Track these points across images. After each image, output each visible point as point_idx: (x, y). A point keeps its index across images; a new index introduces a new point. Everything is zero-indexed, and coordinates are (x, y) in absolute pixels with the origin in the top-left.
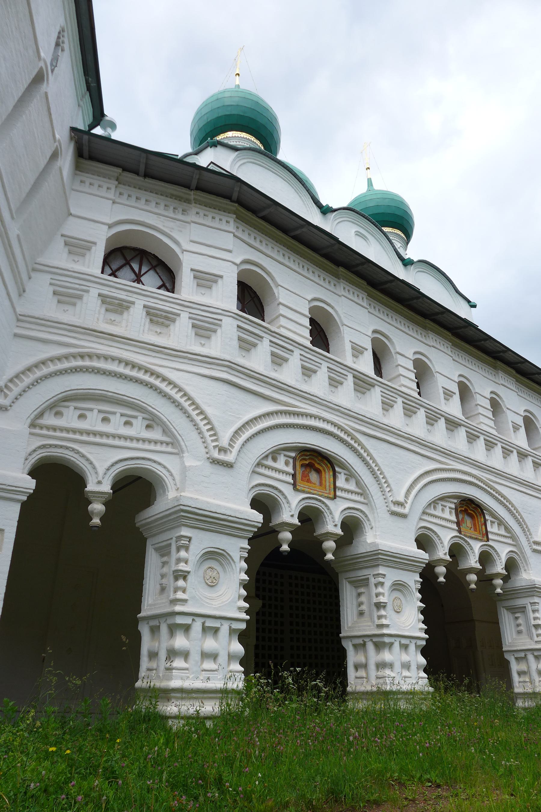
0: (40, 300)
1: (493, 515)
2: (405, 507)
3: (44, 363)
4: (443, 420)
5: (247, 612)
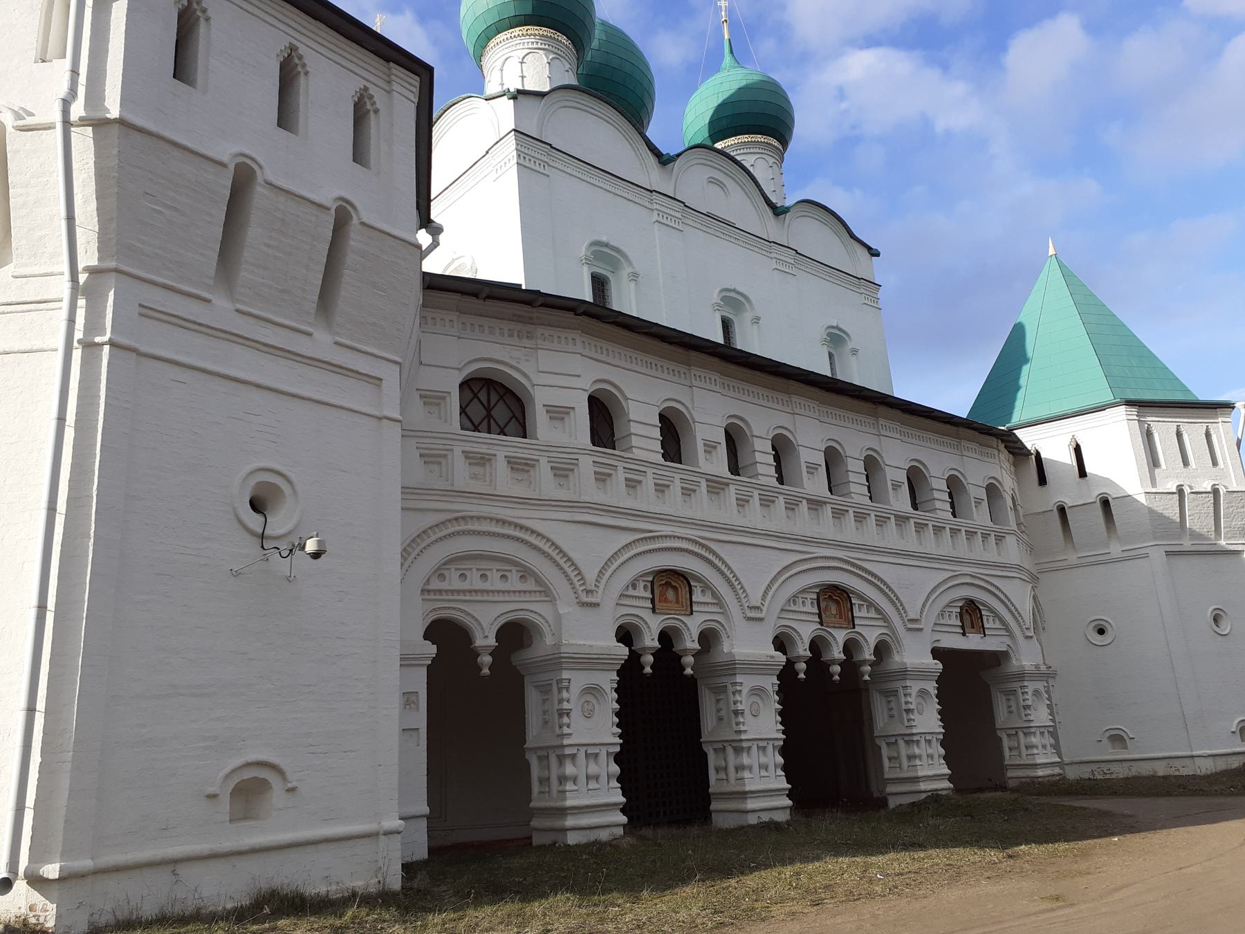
1: (861, 597)
5: (620, 736)
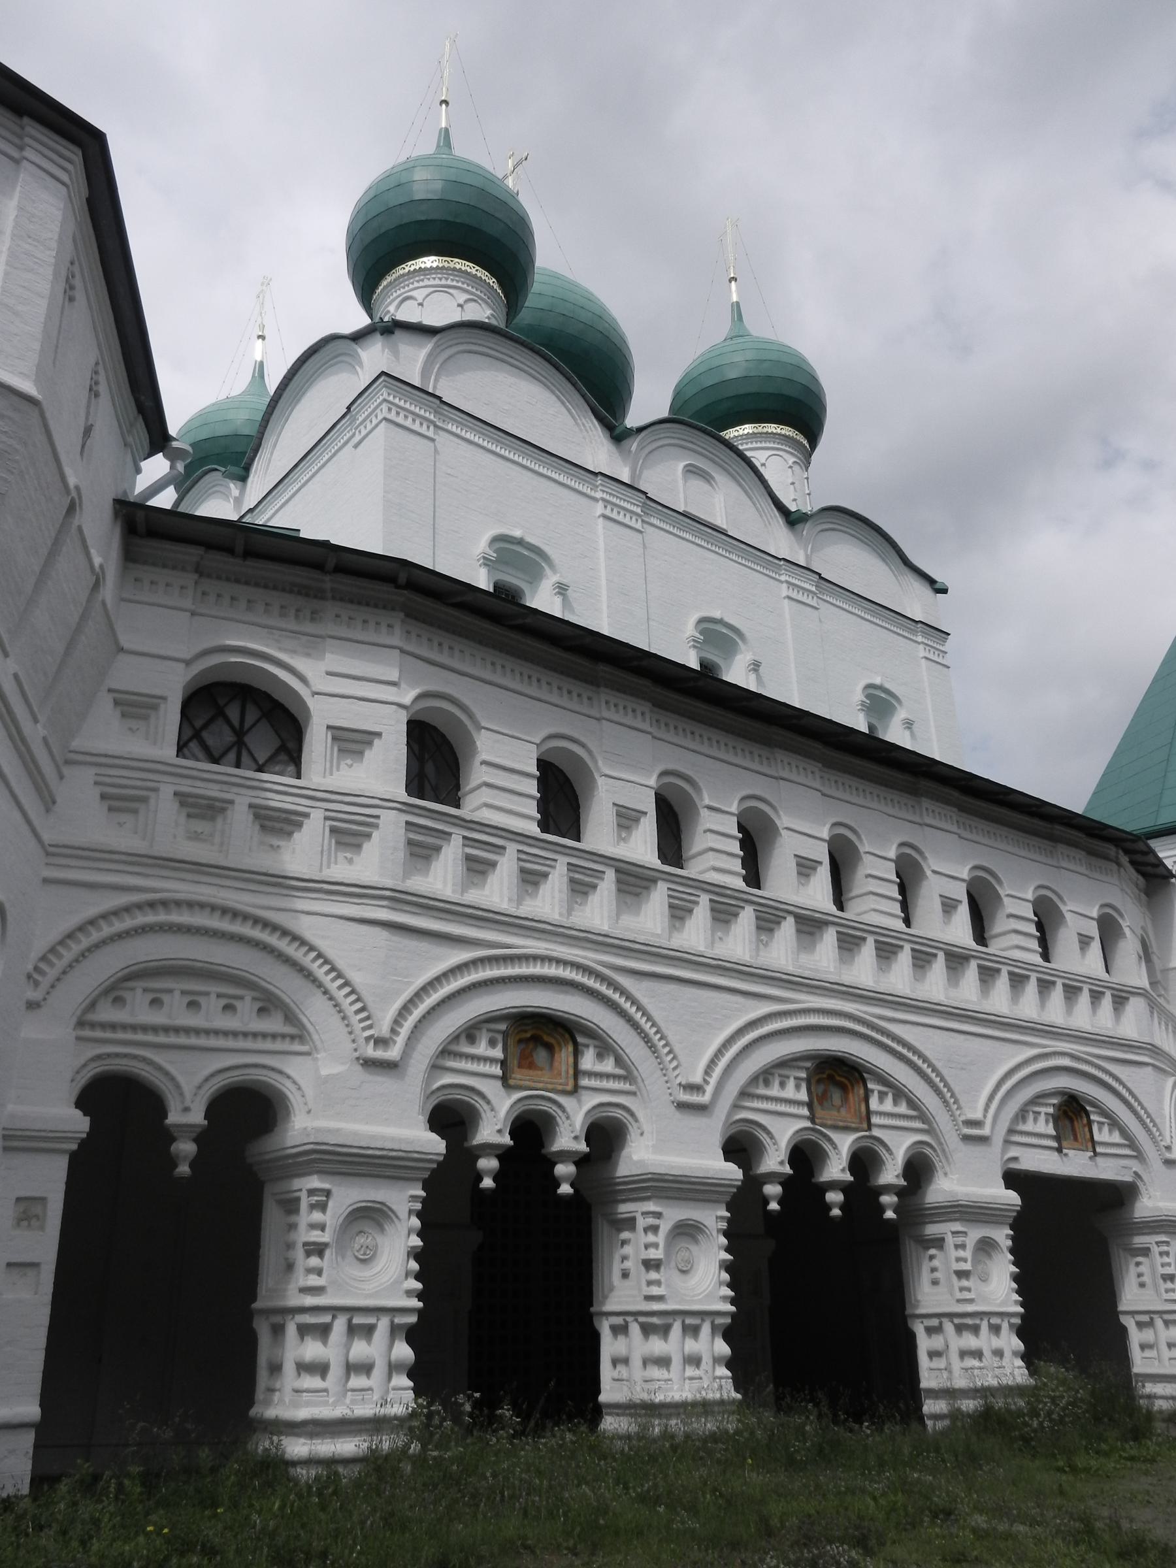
0: (84, 819)
2: (704, 1092)
3: (92, 922)
4: (790, 920)
